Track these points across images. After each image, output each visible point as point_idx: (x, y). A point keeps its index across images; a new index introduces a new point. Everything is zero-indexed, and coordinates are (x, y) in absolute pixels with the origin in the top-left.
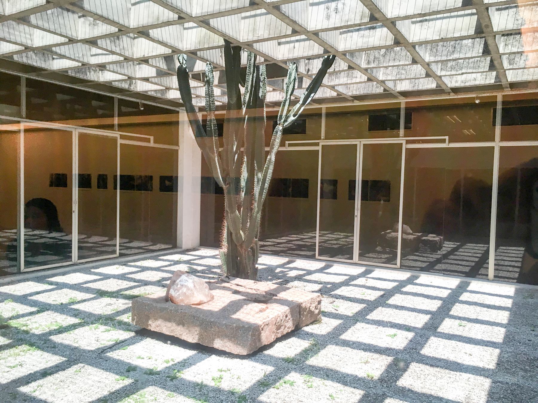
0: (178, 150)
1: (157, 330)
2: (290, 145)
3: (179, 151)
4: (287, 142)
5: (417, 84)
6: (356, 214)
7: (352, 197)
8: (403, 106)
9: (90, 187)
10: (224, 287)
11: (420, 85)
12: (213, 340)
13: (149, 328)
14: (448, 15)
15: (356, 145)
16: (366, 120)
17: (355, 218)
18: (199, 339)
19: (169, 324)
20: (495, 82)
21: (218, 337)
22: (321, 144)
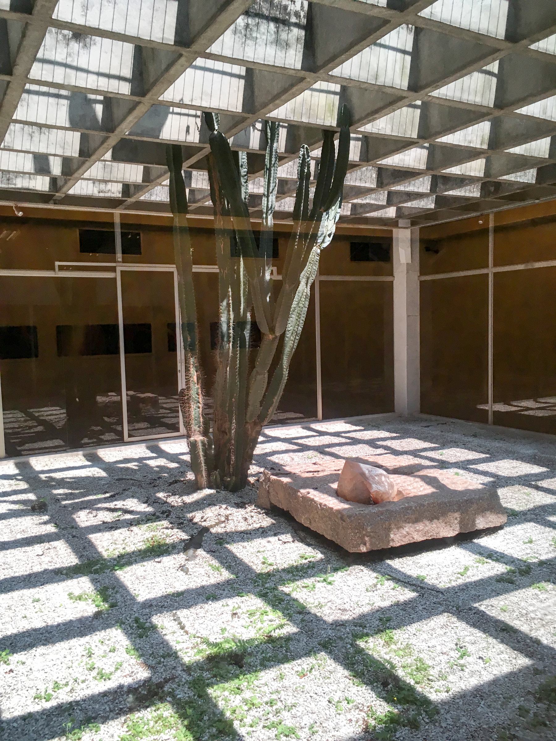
0: (392, 282)
1: (406, 541)
2: (61, 268)
3: (394, 282)
4: (57, 263)
5: (283, 205)
6: (179, 368)
7: (172, 347)
8: (117, 220)
9: (148, 350)
10: (434, 462)
11: (286, 206)
12: (474, 521)
13: (392, 544)
14: (53, 91)
15: (121, 271)
16: (75, 234)
17: (179, 374)
18: (461, 528)
19: (420, 526)
20: (351, 214)
21: (478, 514)
22: (119, 269)
